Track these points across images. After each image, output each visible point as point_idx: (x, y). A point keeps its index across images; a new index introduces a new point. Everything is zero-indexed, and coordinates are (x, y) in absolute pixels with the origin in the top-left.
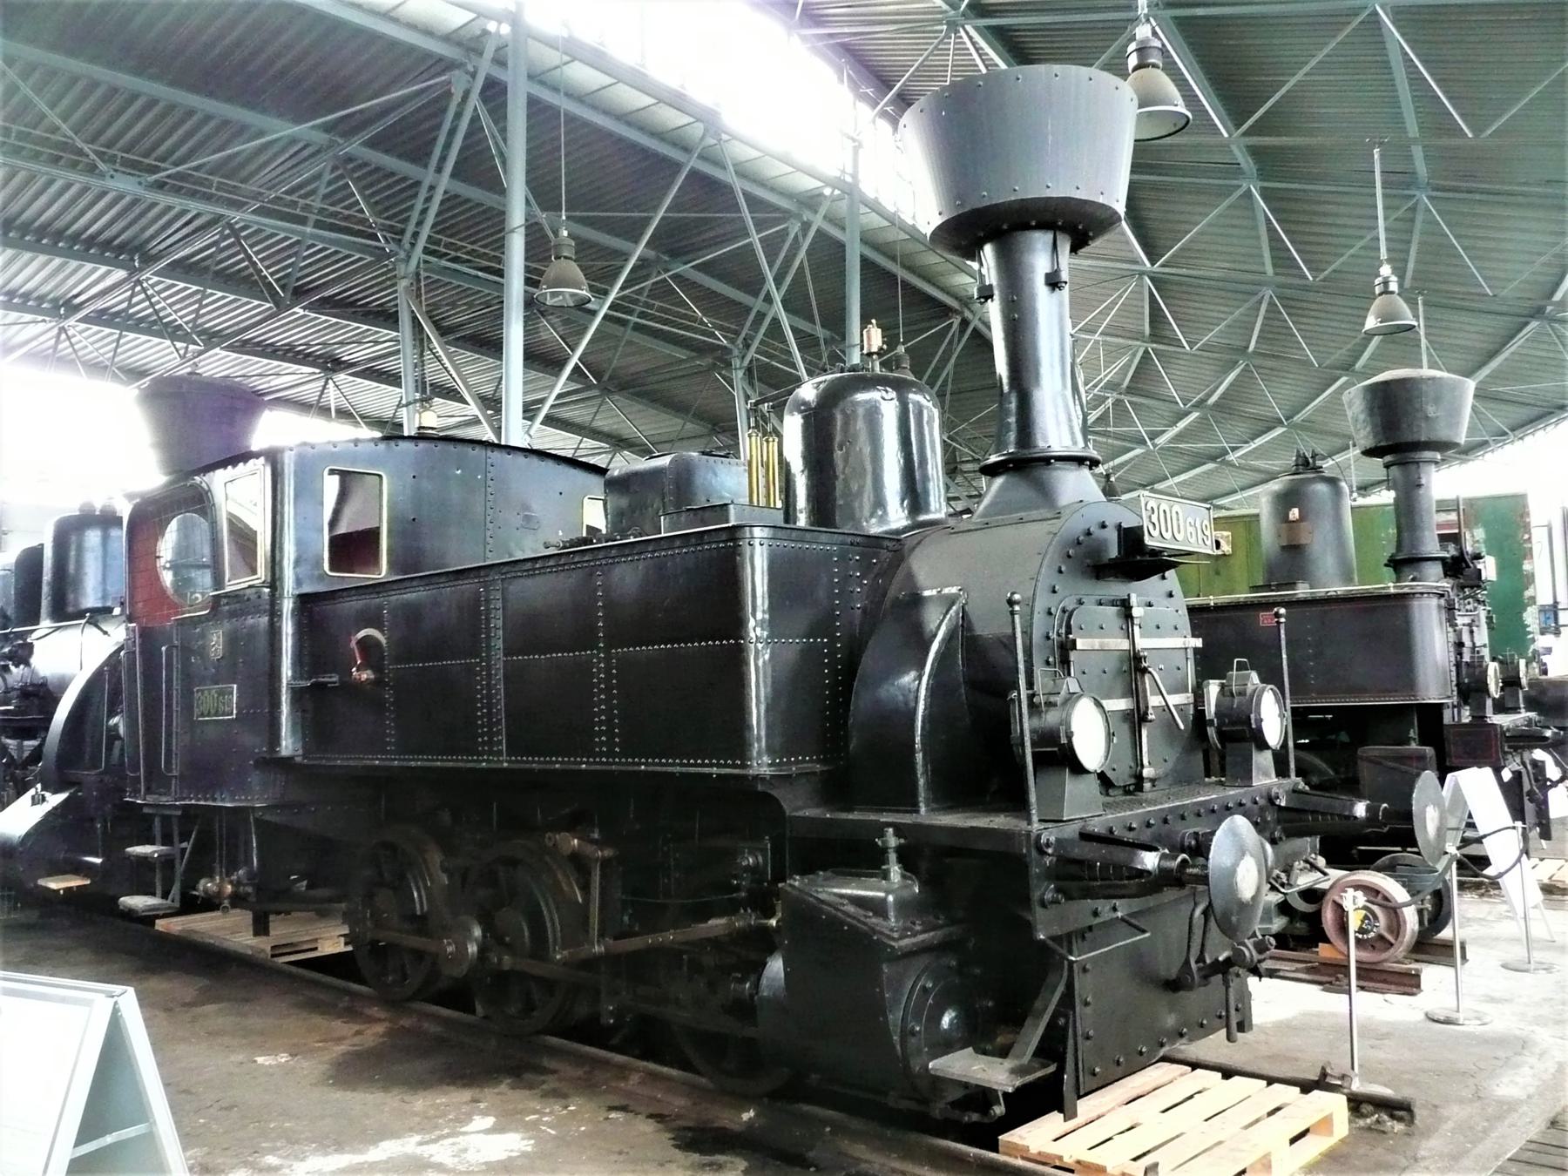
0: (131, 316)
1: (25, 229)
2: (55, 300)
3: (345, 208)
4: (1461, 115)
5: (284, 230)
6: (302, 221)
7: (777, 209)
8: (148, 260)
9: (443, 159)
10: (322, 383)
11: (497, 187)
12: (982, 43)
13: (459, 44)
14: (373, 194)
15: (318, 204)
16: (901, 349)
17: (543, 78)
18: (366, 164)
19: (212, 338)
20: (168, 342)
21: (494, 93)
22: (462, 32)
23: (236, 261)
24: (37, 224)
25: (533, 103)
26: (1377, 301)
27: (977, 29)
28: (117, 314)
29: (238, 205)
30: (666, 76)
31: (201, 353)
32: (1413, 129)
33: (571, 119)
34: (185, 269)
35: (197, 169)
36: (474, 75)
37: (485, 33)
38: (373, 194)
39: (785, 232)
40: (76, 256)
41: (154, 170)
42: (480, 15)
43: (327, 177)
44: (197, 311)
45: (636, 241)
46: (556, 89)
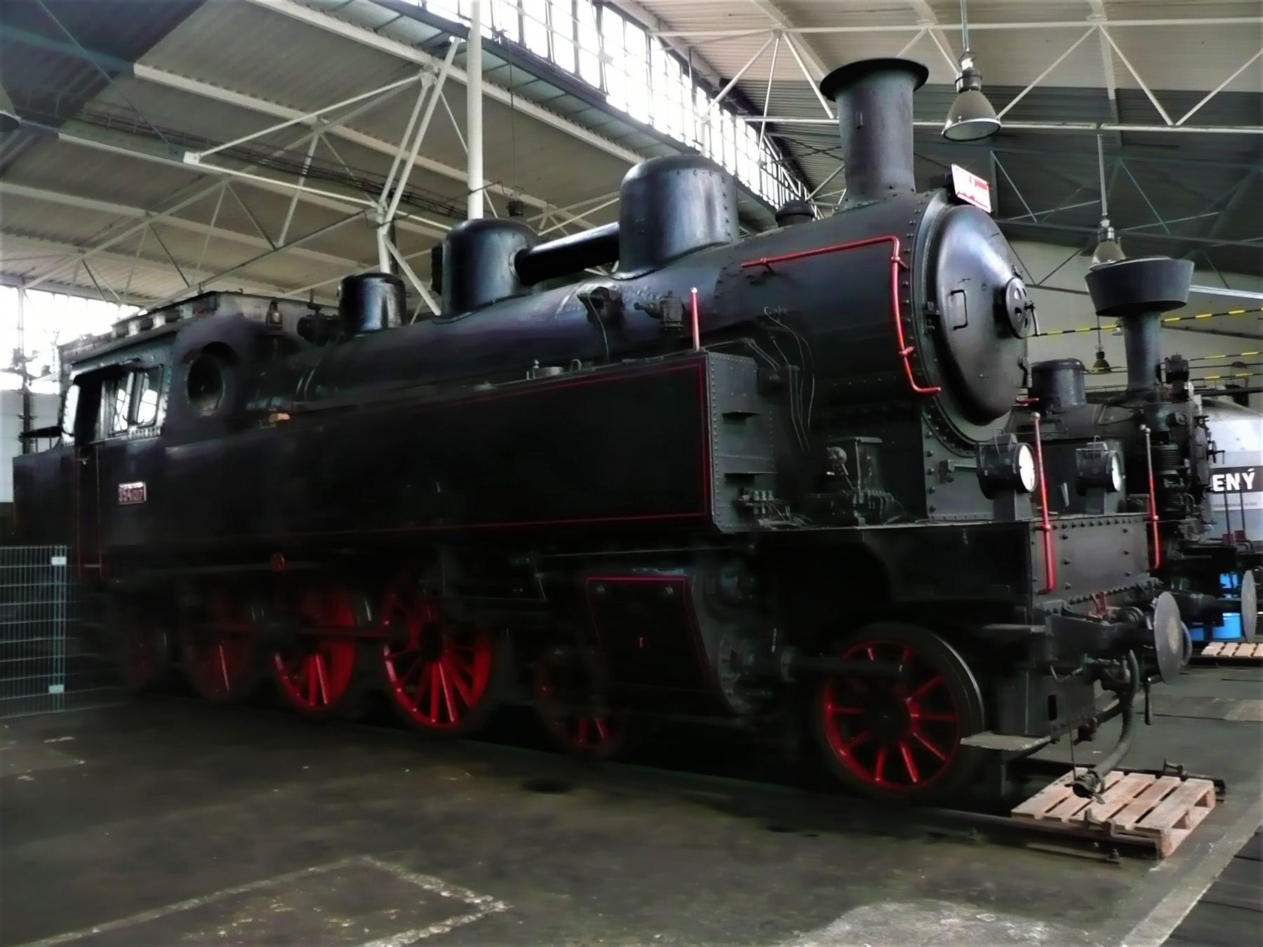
36: (437, 75)
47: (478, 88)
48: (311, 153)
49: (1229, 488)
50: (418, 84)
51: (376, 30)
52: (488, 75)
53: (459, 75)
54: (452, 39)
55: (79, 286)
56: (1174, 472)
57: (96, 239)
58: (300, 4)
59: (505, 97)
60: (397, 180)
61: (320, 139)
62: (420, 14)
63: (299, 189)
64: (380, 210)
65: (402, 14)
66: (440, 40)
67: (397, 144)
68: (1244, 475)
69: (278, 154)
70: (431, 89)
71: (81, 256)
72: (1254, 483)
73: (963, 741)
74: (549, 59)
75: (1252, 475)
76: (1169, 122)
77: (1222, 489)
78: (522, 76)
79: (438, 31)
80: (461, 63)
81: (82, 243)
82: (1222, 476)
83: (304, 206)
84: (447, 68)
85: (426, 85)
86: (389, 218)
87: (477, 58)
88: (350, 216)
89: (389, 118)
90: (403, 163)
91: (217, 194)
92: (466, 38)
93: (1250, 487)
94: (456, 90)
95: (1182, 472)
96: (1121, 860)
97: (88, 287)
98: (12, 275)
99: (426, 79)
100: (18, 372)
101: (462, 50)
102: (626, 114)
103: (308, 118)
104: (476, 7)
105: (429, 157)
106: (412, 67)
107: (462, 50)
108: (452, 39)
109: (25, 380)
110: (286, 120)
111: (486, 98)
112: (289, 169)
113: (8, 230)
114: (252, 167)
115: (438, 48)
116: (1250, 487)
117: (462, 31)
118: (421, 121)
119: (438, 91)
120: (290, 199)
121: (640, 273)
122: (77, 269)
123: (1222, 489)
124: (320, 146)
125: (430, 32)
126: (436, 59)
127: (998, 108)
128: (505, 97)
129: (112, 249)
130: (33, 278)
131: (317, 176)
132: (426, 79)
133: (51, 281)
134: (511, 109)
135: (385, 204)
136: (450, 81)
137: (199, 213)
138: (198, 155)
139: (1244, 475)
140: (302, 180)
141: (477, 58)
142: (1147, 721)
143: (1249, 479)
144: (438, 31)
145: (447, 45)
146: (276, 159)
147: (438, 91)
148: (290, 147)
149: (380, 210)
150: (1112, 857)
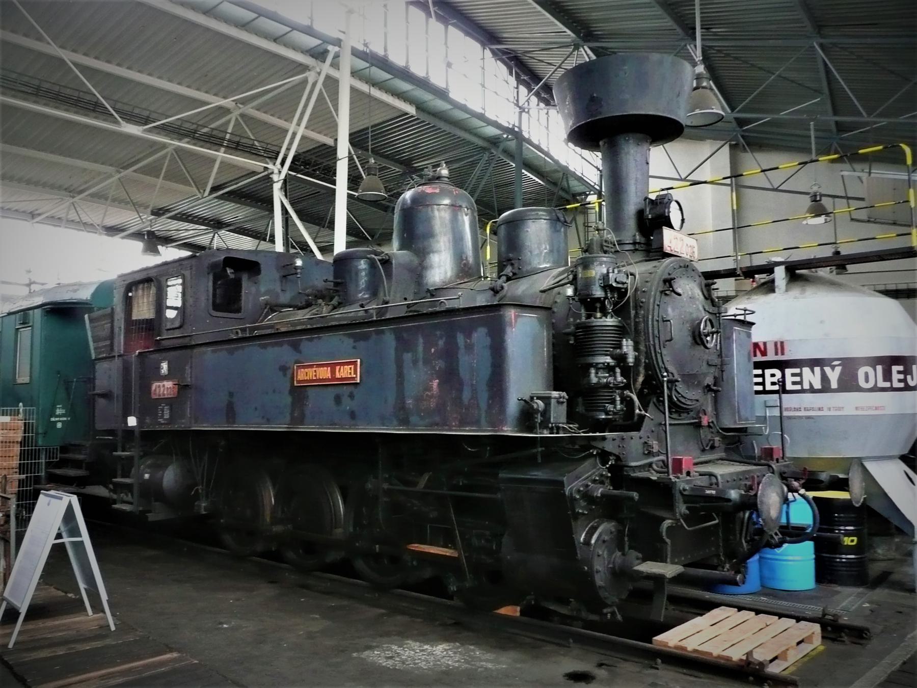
36: (319, 74)
47: (346, 83)
48: (230, 131)
49: (806, 386)
50: (305, 81)
51: (275, 40)
52: (354, 73)
53: (334, 73)
54: (330, 48)
56: (608, 360)
57: (81, 188)
58: (175, 3)
59: (365, 88)
60: (288, 149)
61: (237, 119)
62: (309, 31)
63: (221, 155)
64: (276, 171)
65: (293, 29)
66: (321, 49)
67: (289, 120)
68: (827, 370)
69: (205, 130)
70: (314, 84)
71: (72, 200)
72: (840, 380)
74: (406, 67)
75: (838, 370)
77: (902, 385)
78: (384, 76)
79: (319, 42)
80: (335, 65)
81: (72, 192)
82: (797, 371)
84: (326, 68)
85: (311, 81)
86: (283, 176)
87: (347, 62)
88: (254, 173)
89: (286, 104)
90: (294, 134)
91: (165, 157)
92: (340, 46)
93: (834, 385)
94: (332, 84)
95: (621, 359)
97: (72, 221)
101: (337, 56)
102: (465, 105)
103: (227, 103)
106: (305, 68)
107: (337, 56)
108: (330, 48)
110: (208, 104)
111: (353, 90)
112: (213, 140)
113: (4, 177)
114: (187, 140)
115: (320, 55)
116: (834, 385)
117: (338, 42)
118: (307, 107)
119: (319, 86)
120: (214, 161)
122: (69, 209)
123: (902, 385)
124: (237, 123)
125: (313, 42)
126: (320, 63)
128: (365, 88)
129: (92, 195)
130: (39, 215)
131: (237, 147)
132: (311, 76)
133: (52, 217)
134: (369, 96)
135: (279, 166)
136: (328, 78)
137: (152, 171)
138: (141, 128)
139: (827, 370)
140: (223, 149)
141: (347, 62)
143: (834, 376)
144: (319, 42)
145: (326, 52)
146: (204, 134)
147: (319, 86)
148: (212, 126)
149: (276, 171)
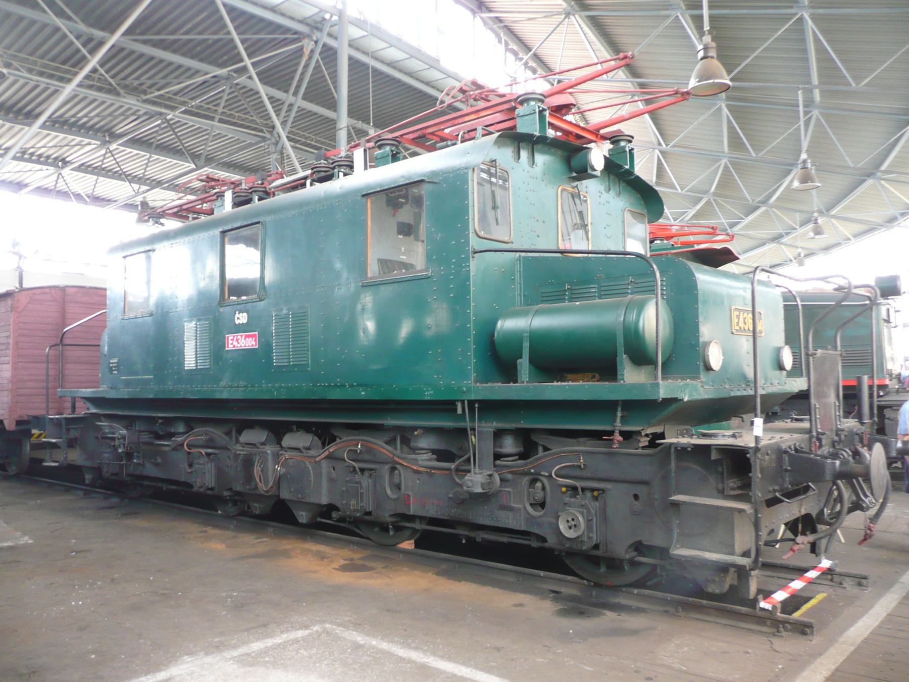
0: (103, 169)
1: (65, 122)
2: (56, 158)
3: (230, 110)
4: (828, 41)
5: (192, 121)
6: (212, 119)
7: (287, 30)
8: (114, 137)
9: (298, 87)
10: (55, 177)
11: (333, 105)
12: (583, 25)
13: (308, 25)
14: (250, 101)
15: (220, 110)
16: (372, 132)
17: (434, 84)
18: (244, 87)
19: (156, 184)
20: (127, 183)
21: (330, 54)
22: (421, 73)
23: (167, 137)
24: (98, 126)
25: (353, 62)
26: (698, 66)
27: (580, 17)
28: (96, 168)
29: (173, 108)
30: (412, 39)
31: (148, 191)
32: (815, 80)
33: (375, 70)
34: (138, 142)
35: (167, 93)
36: (316, 42)
37: (324, 19)
38: (250, 101)
39: (301, 49)
40: (9, 121)
41: (145, 92)
42: (321, 10)
43: (228, 91)
44: (147, 164)
45: (113, 32)
46: (365, 53)
55: (59, 192)
73: (190, 361)
76: (854, 85)
83: (102, 63)
85: (307, 52)
96: (784, 634)
98: (11, 182)
99: (308, 45)
100: (16, 253)
104: (344, 3)
105: (311, 101)
109: (20, 258)
111: (350, 58)
119: (317, 56)
121: (660, 328)
127: (729, 72)
142: (497, 224)
147: (317, 56)
150: (778, 632)
